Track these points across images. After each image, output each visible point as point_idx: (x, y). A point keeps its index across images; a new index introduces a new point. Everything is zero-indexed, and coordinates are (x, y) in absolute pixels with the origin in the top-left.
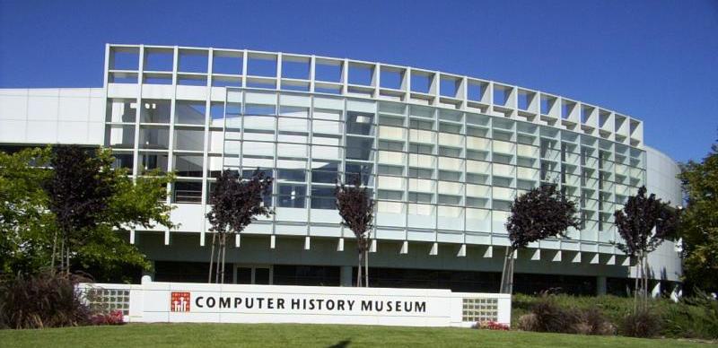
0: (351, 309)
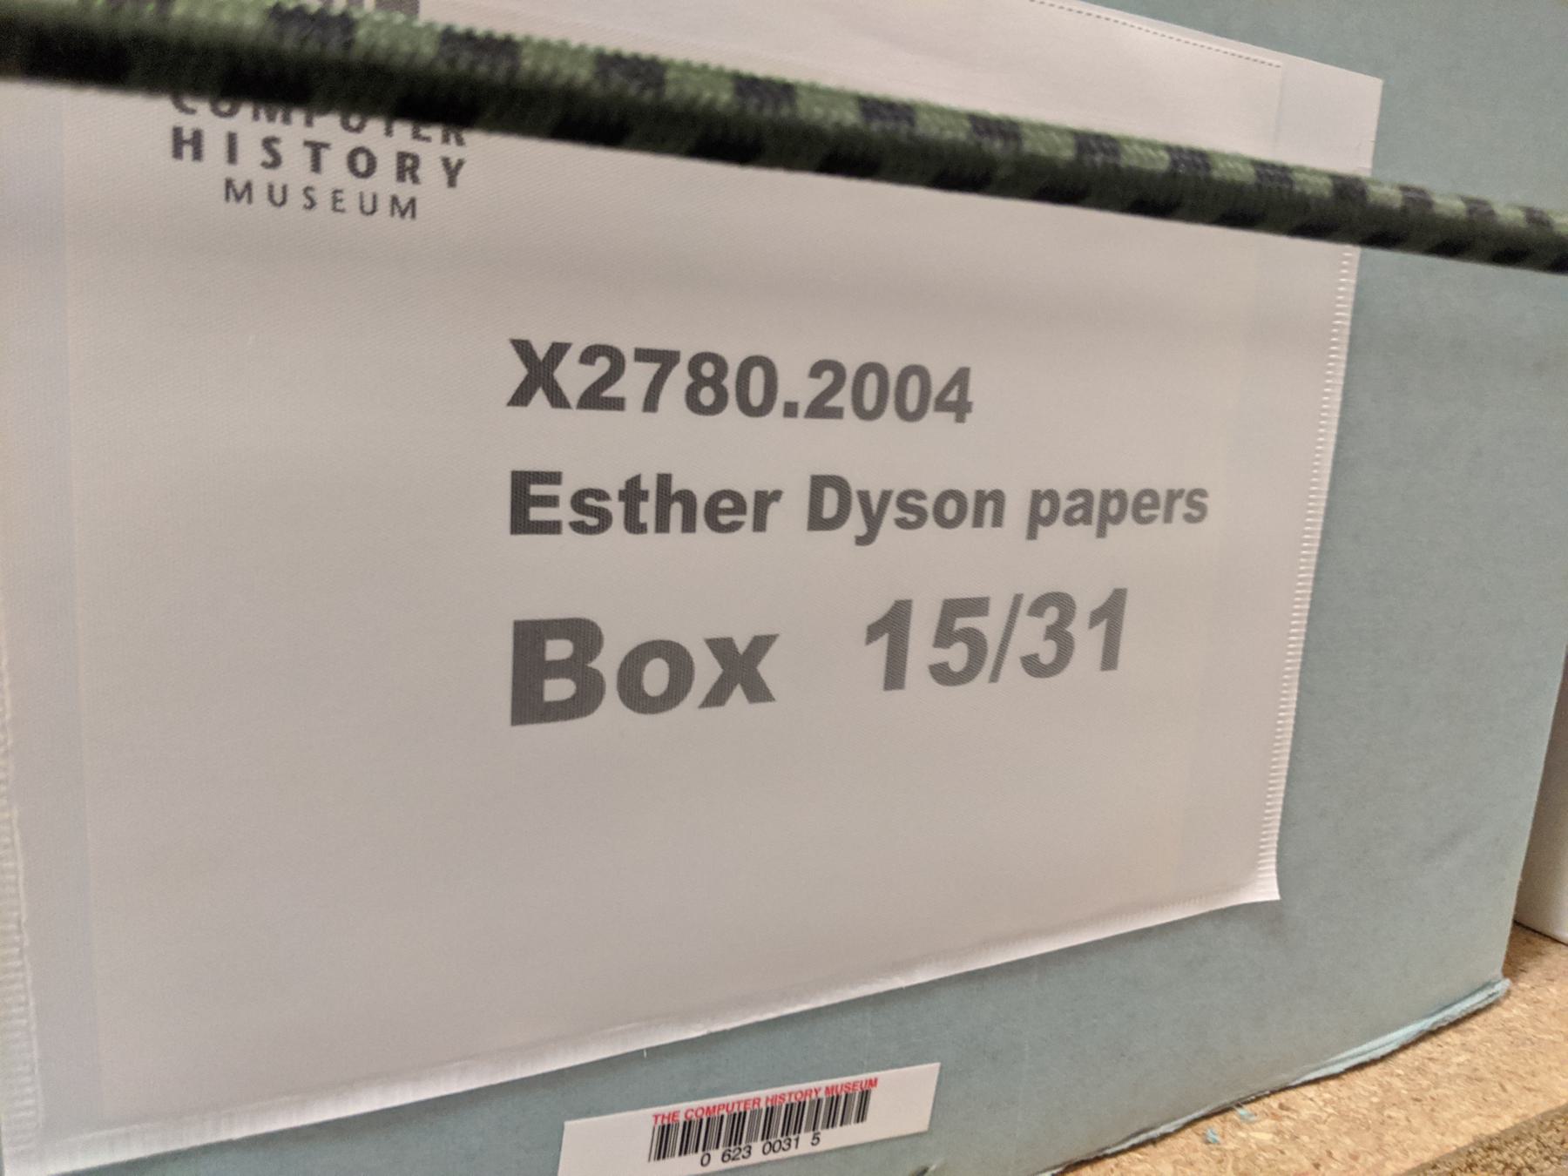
0: (452, 183)
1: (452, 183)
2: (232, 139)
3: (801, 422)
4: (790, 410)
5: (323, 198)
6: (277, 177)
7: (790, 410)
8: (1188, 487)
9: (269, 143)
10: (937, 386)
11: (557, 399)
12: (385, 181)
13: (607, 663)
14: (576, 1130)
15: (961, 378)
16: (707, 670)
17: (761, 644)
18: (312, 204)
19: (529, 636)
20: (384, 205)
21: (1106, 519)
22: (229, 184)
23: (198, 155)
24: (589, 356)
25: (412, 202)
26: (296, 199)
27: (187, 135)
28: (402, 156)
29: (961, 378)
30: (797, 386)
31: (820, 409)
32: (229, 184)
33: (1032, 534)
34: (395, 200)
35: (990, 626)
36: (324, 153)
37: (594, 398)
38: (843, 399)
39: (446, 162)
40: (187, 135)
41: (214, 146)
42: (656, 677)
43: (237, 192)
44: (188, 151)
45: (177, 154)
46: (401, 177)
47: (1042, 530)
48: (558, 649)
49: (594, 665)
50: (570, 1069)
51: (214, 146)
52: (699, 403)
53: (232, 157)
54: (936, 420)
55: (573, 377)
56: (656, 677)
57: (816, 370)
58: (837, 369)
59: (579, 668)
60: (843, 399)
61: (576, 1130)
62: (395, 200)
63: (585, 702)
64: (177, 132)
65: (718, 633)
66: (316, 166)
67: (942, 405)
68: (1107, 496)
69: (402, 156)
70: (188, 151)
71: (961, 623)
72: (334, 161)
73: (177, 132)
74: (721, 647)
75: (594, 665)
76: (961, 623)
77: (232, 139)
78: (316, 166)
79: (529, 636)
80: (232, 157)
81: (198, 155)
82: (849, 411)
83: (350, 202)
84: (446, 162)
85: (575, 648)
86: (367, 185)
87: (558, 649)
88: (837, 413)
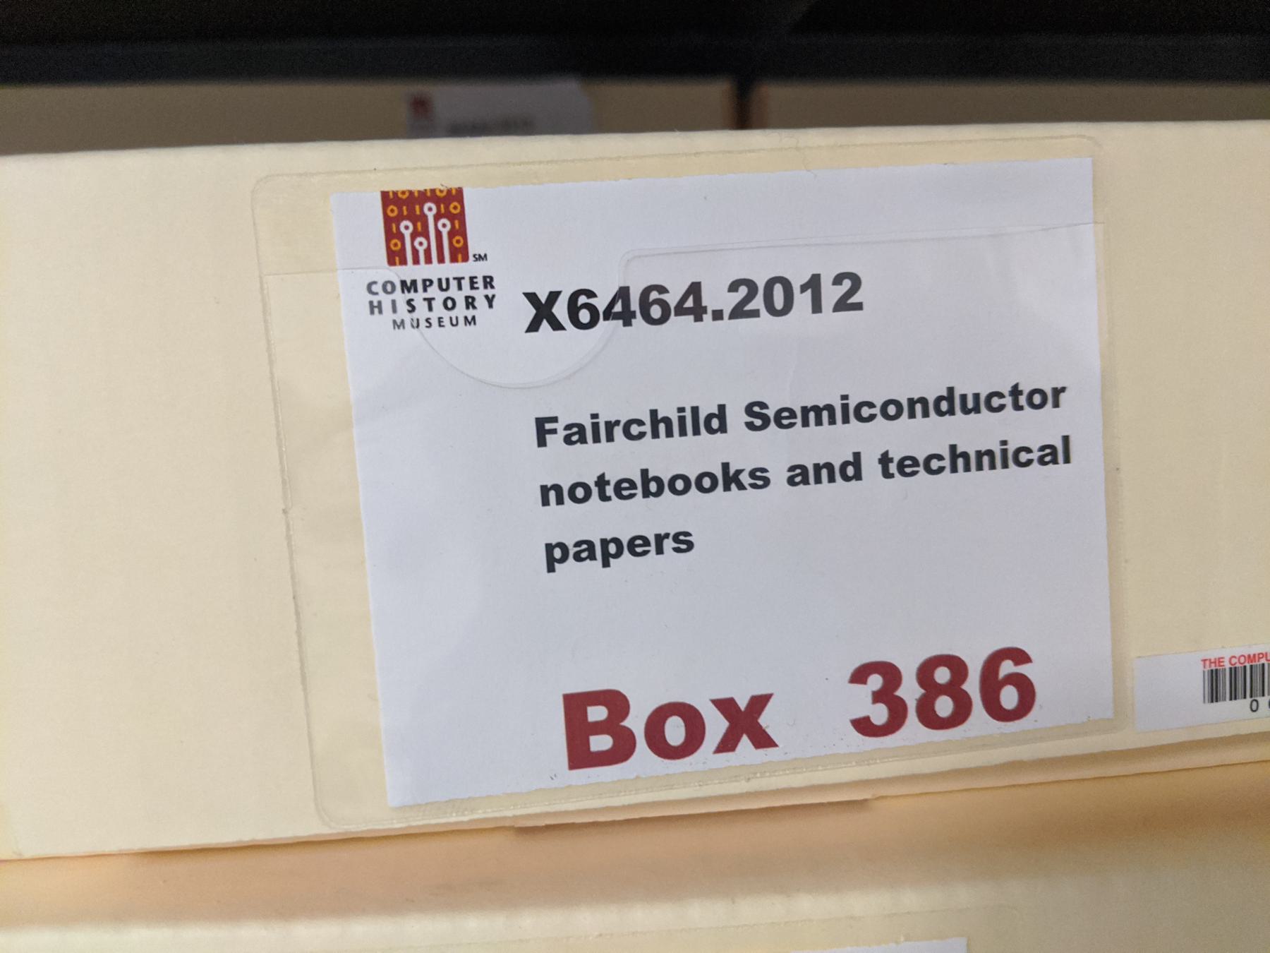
0: (491, 306)
1: (491, 306)
2: (394, 302)
4: (718, 315)
5: (435, 322)
6: (415, 315)
7: (718, 315)
9: (409, 302)
12: (461, 311)
13: (636, 722)
16: (716, 726)
17: (759, 702)
18: (430, 325)
19: (575, 705)
20: (461, 321)
22: (395, 322)
23: (380, 312)
25: (474, 318)
26: (423, 324)
27: (375, 304)
28: (467, 298)
31: (739, 312)
32: (395, 322)
33: (551, 569)
34: (466, 318)
36: (433, 303)
38: (758, 303)
39: (487, 297)
40: (375, 304)
41: (387, 306)
42: (675, 731)
43: (399, 325)
44: (376, 310)
45: (372, 312)
46: (468, 308)
49: (626, 723)
51: (387, 306)
52: (649, 314)
53: (395, 311)
56: (675, 731)
57: (734, 287)
58: (751, 285)
59: (614, 725)
60: (758, 303)
62: (466, 318)
63: (622, 751)
64: (371, 303)
66: (430, 309)
69: (467, 298)
70: (376, 310)
72: (437, 305)
73: (371, 303)
74: (726, 706)
75: (626, 723)
77: (394, 302)
78: (430, 309)
79: (575, 705)
80: (395, 311)
81: (380, 312)
82: (763, 312)
83: (446, 322)
84: (487, 297)
85: (614, 745)
86: (453, 314)
87: (597, 713)
88: (755, 314)
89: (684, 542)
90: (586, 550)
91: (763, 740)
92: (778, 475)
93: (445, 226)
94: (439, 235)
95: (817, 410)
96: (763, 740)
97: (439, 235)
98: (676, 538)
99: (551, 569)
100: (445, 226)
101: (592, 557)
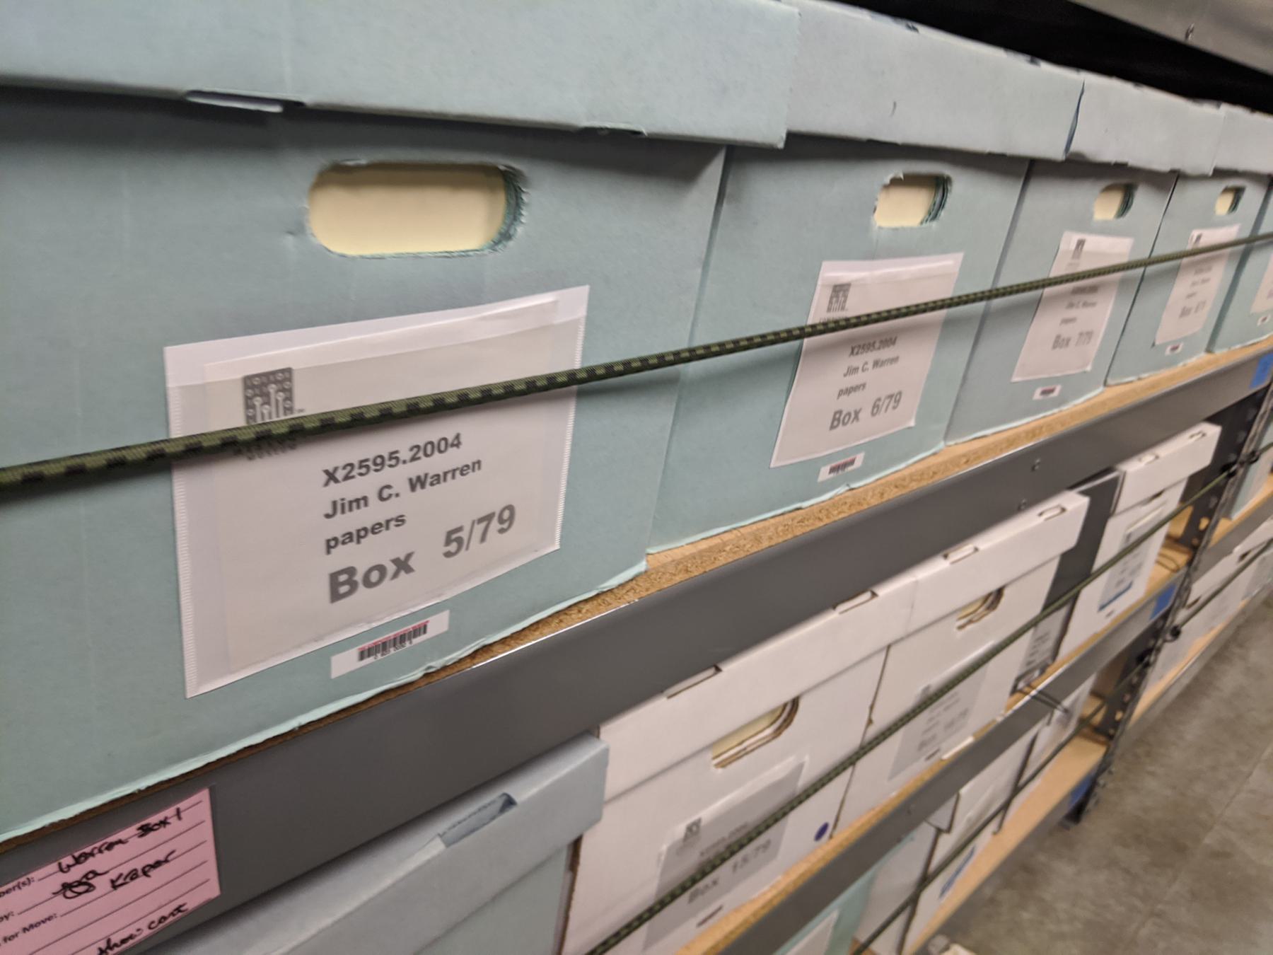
3: (409, 464)
4: (404, 462)
7: (404, 462)
8: (394, 515)
10: (450, 441)
11: (336, 481)
13: (359, 577)
14: (212, 890)
15: (458, 437)
16: (391, 569)
21: (359, 537)
24: (344, 468)
29: (458, 437)
30: (405, 454)
31: (414, 459)
33: (328, 552)
35: (464, 534)
37: (347, 478)
38: (421, 454)
47: (333, 551)
48: (343, 578)
50: (183, 776)
54: (451, 450)
55: (340, 474)
57: (411, 449)
60: (421, 454)
61: (212, 890)
65: (393, 557)
67: (453, 445)
68: (358, 531)
71: (454, 536)
74: (396, 561)
76: (454, 536)
87: (343, 578)
89: (400, 520)
90: (349, 537)
91: (327, 472)
92: (373, 498)
93: (281, 396)
94: (277, 401)
95: (357, 501)
96: (327, 472)
97: (277, 401)
98: (397, 520)
99: (328, 552)
100: (281, 396)
101: (351, 541)
